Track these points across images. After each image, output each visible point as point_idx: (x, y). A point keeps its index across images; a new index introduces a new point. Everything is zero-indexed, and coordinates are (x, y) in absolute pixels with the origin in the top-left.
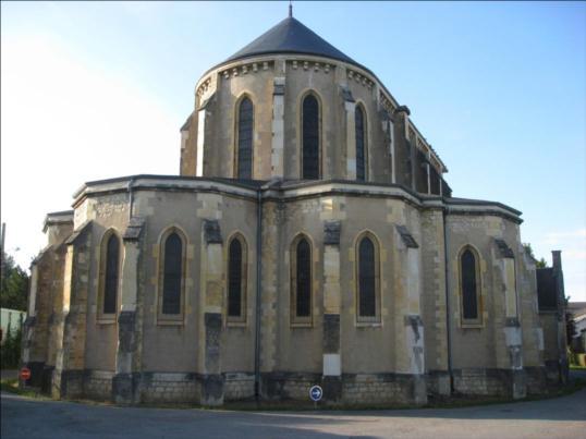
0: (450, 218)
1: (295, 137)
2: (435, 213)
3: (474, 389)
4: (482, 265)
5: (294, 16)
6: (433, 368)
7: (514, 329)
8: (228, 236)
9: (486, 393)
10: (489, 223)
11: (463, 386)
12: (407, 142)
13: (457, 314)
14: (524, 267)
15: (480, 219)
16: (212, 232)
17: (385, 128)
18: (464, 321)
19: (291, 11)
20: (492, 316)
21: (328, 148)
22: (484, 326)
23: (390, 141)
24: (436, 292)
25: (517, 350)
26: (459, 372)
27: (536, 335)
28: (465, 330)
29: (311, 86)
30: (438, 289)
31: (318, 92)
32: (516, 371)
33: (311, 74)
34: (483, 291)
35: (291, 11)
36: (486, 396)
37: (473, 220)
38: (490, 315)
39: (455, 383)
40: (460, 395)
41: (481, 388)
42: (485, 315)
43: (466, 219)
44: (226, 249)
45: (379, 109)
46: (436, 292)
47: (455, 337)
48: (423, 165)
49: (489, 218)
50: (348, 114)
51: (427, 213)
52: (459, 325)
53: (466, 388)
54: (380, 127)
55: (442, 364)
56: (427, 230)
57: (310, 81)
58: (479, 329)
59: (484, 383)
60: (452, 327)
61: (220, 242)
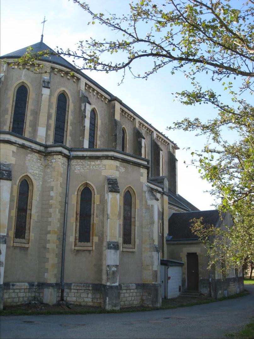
0: (74, 162)
1: (7, 114)
2: (55, 156)
3: (81, 300)
4: (96, 198)
5: (44, 42)
6: (42, 281)
7: (113, 251)
8: (123, 189)
9: (91, 304)
10: (105, 165)
11: (71, 297)
12: (115, 121)
13: (72, 238)
14: (146, 202)
15: (98, 162)
16: (113, 185)
17: (83, 108)
18: (79, 244)
19: (42, 39)
20: (101, 240)
21: (30, 121)
22: (94, 247)
23: (85, 117)
24: (50, 219)
25: (114, 269)
26: (69, 286)
27: (152, 257)
28: (78, 251)
29: (23, 79)
30: (51, 217)
31: (29, 84)
32: (111, 287)
33: (24, 72)
34: (95, 220)
35: (42, 39)
36: (90, 306)
37: (93, 163)
38: (99, 240)
39: (65, 294)
40: (68, 305)
41: (86, 300)
42: (96, 239)
43: (87, 162)
44: (16, 188)
45: (81, 96)
46: (50, 219)
47: (69, 256)
48: (139, 140)
49: (105, 162)
50: (44, 96)
51: (49, 158)
52: (73, 247)
53: (74, 299)
54: (80, 107)
55: (51, 277)
56: (49, 170)
57: (68, 88)
58: (89, 251)
59: (90, 295)
60: (67, 248)
61: (117, 191)
